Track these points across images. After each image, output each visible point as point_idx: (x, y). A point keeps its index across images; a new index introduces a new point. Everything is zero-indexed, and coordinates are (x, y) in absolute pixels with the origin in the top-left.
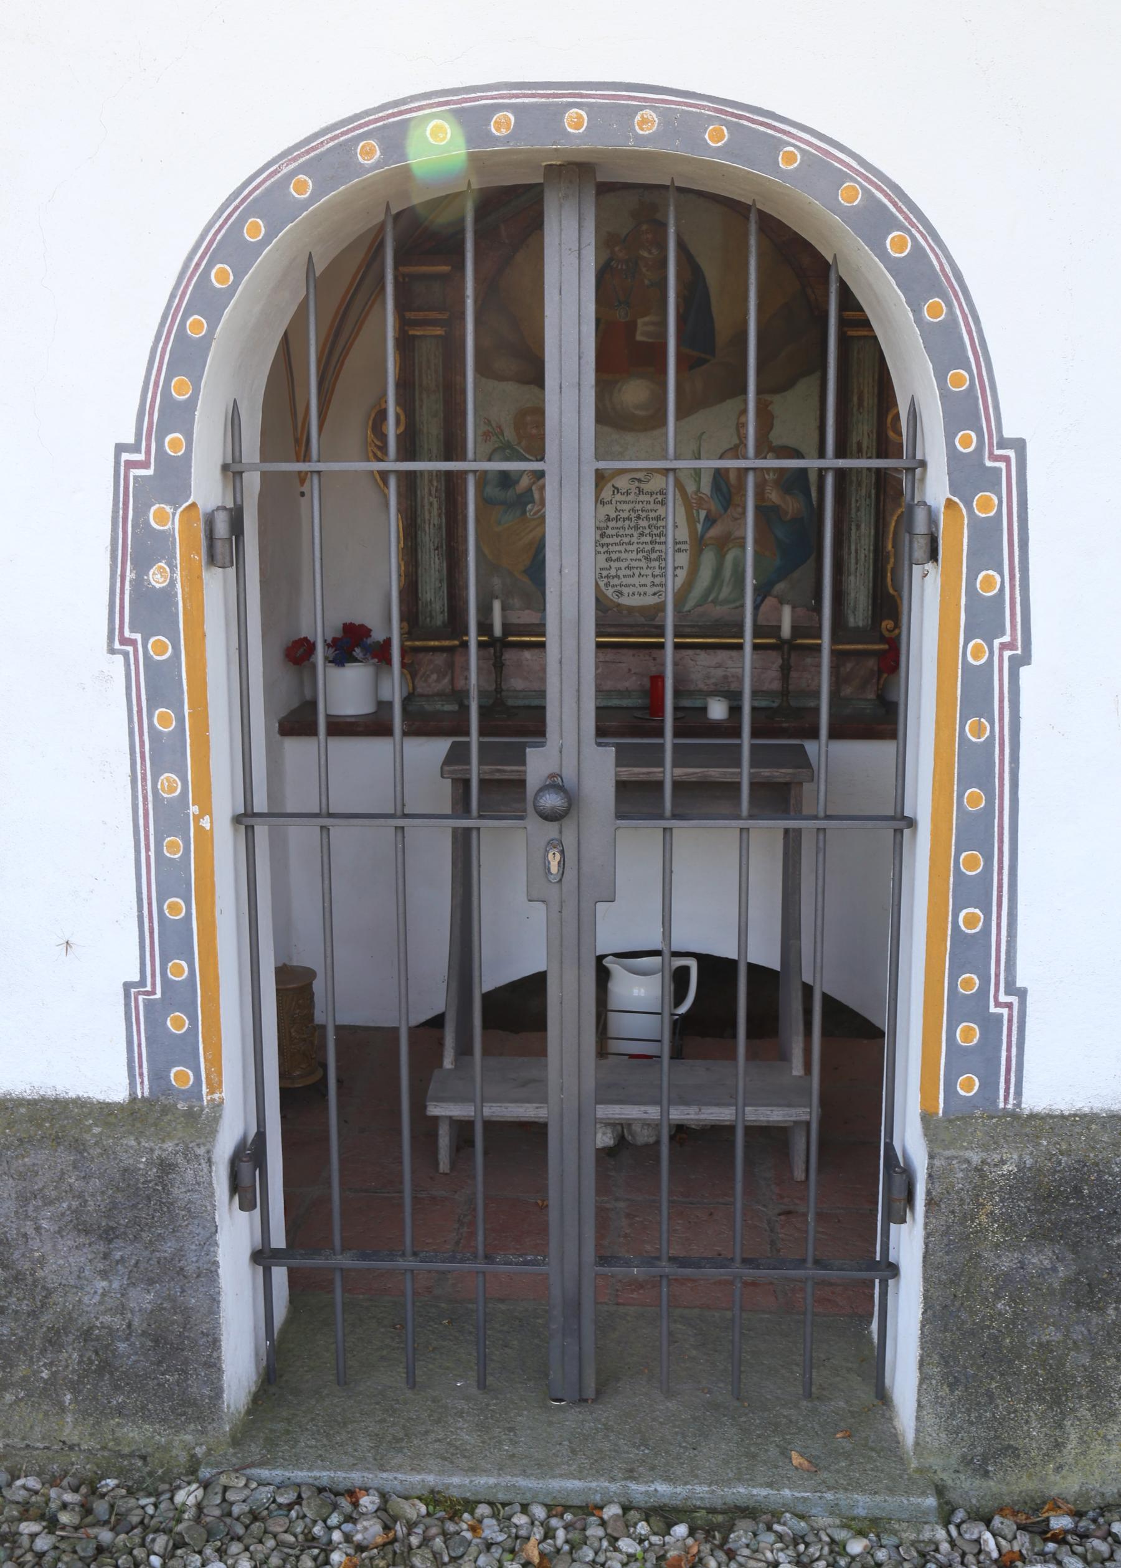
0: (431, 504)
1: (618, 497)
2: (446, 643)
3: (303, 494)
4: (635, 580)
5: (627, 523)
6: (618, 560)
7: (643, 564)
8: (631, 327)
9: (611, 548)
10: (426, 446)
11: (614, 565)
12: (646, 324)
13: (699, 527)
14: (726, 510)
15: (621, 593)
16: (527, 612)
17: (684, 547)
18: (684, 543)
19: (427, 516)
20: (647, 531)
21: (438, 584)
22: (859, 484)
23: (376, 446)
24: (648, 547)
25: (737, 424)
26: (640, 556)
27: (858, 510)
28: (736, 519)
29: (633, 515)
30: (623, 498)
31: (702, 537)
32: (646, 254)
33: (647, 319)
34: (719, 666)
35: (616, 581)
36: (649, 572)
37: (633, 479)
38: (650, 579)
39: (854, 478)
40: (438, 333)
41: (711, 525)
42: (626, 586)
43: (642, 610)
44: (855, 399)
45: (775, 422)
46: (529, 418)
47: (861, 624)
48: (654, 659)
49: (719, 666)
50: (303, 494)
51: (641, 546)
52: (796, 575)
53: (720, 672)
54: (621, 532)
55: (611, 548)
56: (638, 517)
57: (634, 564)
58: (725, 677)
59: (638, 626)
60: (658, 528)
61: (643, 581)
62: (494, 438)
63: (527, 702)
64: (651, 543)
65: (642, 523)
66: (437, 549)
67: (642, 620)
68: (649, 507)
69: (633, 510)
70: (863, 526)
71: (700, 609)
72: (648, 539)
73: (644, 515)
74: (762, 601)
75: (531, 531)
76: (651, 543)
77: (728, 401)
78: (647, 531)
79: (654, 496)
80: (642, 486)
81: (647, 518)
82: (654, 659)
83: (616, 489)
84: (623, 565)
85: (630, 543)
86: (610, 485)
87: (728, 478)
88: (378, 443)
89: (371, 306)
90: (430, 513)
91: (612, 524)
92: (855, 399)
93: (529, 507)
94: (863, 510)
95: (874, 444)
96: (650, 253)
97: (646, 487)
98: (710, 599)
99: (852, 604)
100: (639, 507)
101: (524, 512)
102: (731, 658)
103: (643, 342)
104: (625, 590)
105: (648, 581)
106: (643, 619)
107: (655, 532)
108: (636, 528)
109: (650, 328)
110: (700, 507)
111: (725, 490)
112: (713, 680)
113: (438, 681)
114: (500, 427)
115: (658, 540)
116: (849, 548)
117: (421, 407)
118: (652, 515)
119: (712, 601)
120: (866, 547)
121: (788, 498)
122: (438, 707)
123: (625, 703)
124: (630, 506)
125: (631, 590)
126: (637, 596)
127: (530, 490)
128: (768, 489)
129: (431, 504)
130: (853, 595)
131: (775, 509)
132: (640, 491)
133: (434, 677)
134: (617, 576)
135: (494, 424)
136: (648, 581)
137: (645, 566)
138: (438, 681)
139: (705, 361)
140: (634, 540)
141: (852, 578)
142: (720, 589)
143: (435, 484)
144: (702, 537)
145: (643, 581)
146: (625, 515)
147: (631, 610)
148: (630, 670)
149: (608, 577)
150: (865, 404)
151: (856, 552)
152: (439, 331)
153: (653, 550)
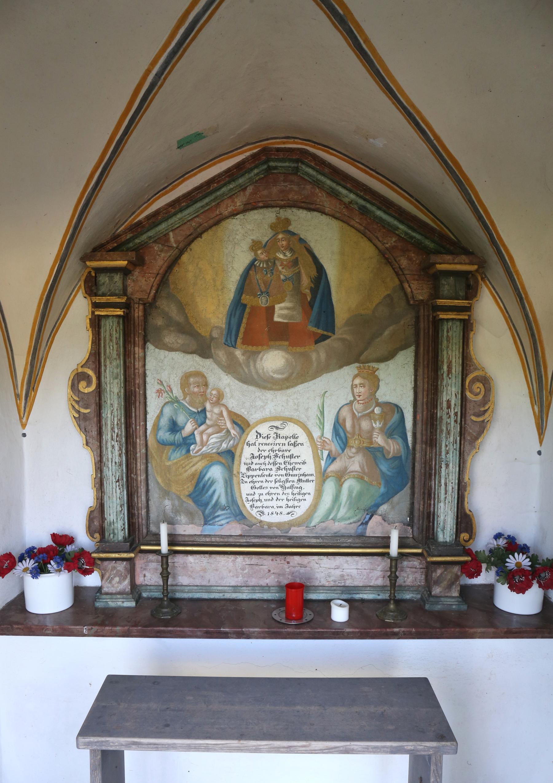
0: (113, 447)
1: (261, 440)
2: (125, 555)
3: (24, 435)
4: (274, 503)
5: (267, 460)
6: (261, 488)
7: (280, 491)
8: (270, 310)
9: (255, 479)
10: (109, 402)
11: (258, 491)
12: (281, 309)
13: (323, 463)
14: (343, 450)
15: (263, 513)
16: (191, 526)
17: (310, 478)
18: (312, 475)
19: (110, 457)
20: (283, 466)
21: (119, 509)
22: (448, 433)
23: (74, 400)
24: (284, 478)
25: (352, 385)
26: (277, 485)
27: (447, 453)
28: (351, 457)
29: (272, 454)
30: (265, 441)
31: (325, 471)
32: (281, 256)
33: (282, 305)
34: (337, 568)
35: (259, 504)
36: (284, 497)
37: (272, 427)
38: (285, 502)
39: (444, 428)
40: (119, 313)
41: (333, 461)
42: (267, 507)
43: (279, 525)
44: (445, 368)
45: (380, 383)
46: (192, 380)
47: (448, 540)
48: (288, 563)
49: (337, 568)
50: (24, 435)
51: (278, 478)
52: (396, 499)
53: (338, 572)
54: (263, 467)
55: (255, 479)
56: (276, 456)
57: (273, 491)
58: (342, 576)
59: (276, 537)
60: (291, 464)
61: (280, 503)
62: (165, 395)
63: (190, 595)
64: (286, 475)
65: (279, 460)
66: (118, 481)
67: (279, 533)
68: (284, 448)
69: (272, 450)
70: (451, 465)
71: (323, 525)
72: (284, 472)
73: (280, 454)
74: (370, 519)
75: (194, 465)
76: (286, 475)
77: (345, 367)
78: (283, 466)
79: (288, 440)
80: (279, 432)
81: (283, 456)
82: (288, 563)
83: (259, 435)
84: (264, 491)
85: (269, 475)
86: (254, 431)
87: (345, 426)
88: (76, 399)
89: (75, 296)
90: (112, 453)
91: (256, 461)
92: (445, 368)
93: (192, 447)
94: (451, 453)
95: (460, 402)
96: (285, 255)
97: (281, 433)
98: (331, 517)
99: (442, 524)
100: (276, 448)
101: (188, 451)
102: (347, 561)
103: (280, 322)
104: (266, 511)
105: (283, 503)
106: (279, 532)
107: (289, 467)
108: (275, 464)
109: (285, 312)
110: (323, 448)
111: (342, 434)
112: (332, 578)
113: (120, 582)
114: (169, 386)
115: (291, 472)
116: (440, 482)
117: (105, 371)
118: (287, 454)
119: (332, 519)
120: (453, 481)
121: (390, 441)
122: (120, 604)
123: (266, 596)
124: (270, 447)
125: (270, 510)
126: (275, 515)
127: (193, 434)
128: (375, 434)
129: (113, 447)
130: (442, 518)
131: (381, 449)
132: (278, 436)
133: (117, 579)
134: (260, 500)
135: (165, 385)
136: (283, 503)
137: (281, 493)
138: (120, 582)
139: (327, 337)
140: (272, 472)
141: (442, 505)
142: (338, 510)
143: (116, 431)
144: (325, 471)
145: (280, 503)
146: (266, 454)
147: (270, 525)
148: (269, 571)
149: (252, 500)
150: (453, 371)
151: (446, 485)
152: (120, 312)
153: (287, 481)
